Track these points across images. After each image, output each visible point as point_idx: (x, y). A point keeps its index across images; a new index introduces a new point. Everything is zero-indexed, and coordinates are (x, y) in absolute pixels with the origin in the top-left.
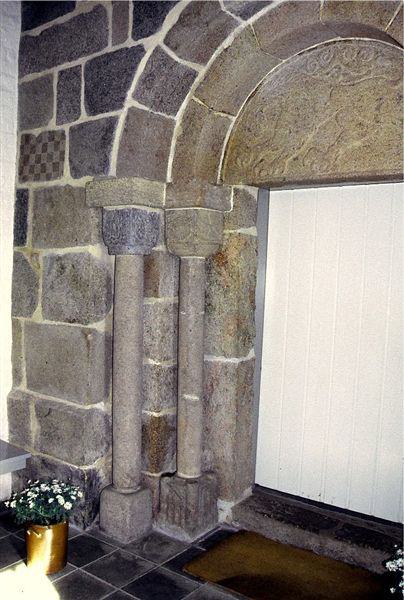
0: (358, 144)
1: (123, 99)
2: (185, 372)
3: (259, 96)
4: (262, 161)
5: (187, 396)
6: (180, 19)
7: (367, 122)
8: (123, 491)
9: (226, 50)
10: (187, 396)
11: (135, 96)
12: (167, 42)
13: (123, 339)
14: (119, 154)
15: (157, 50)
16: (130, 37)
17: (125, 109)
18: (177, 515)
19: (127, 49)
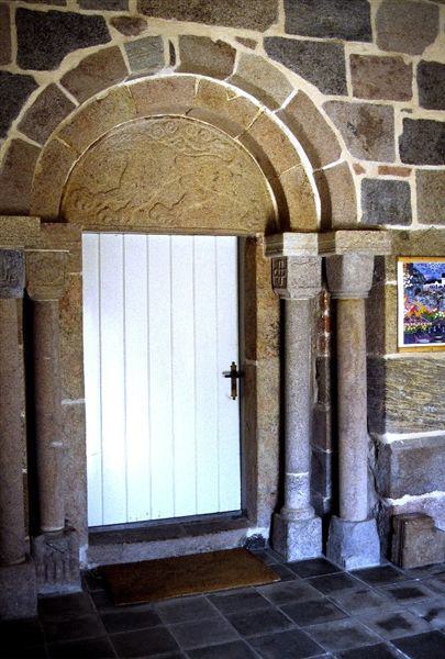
0: (198, 205)
1: (7, 128)
2: (52, 418)
3: (103, 147)
4: (106, 208)
5: (55, 444)
6: (80, 66)
7: (206, 188)
8: (18, 562)
9: (99, 101)
10: (55, 444)
11: (21, 128)
12: (62, 81)
13: (11, 392)
14: (314, 203)
15: (52, 87)
16: (14, 61)
17: (9, 140)
18: (59, 571)
19: (10, 74)
